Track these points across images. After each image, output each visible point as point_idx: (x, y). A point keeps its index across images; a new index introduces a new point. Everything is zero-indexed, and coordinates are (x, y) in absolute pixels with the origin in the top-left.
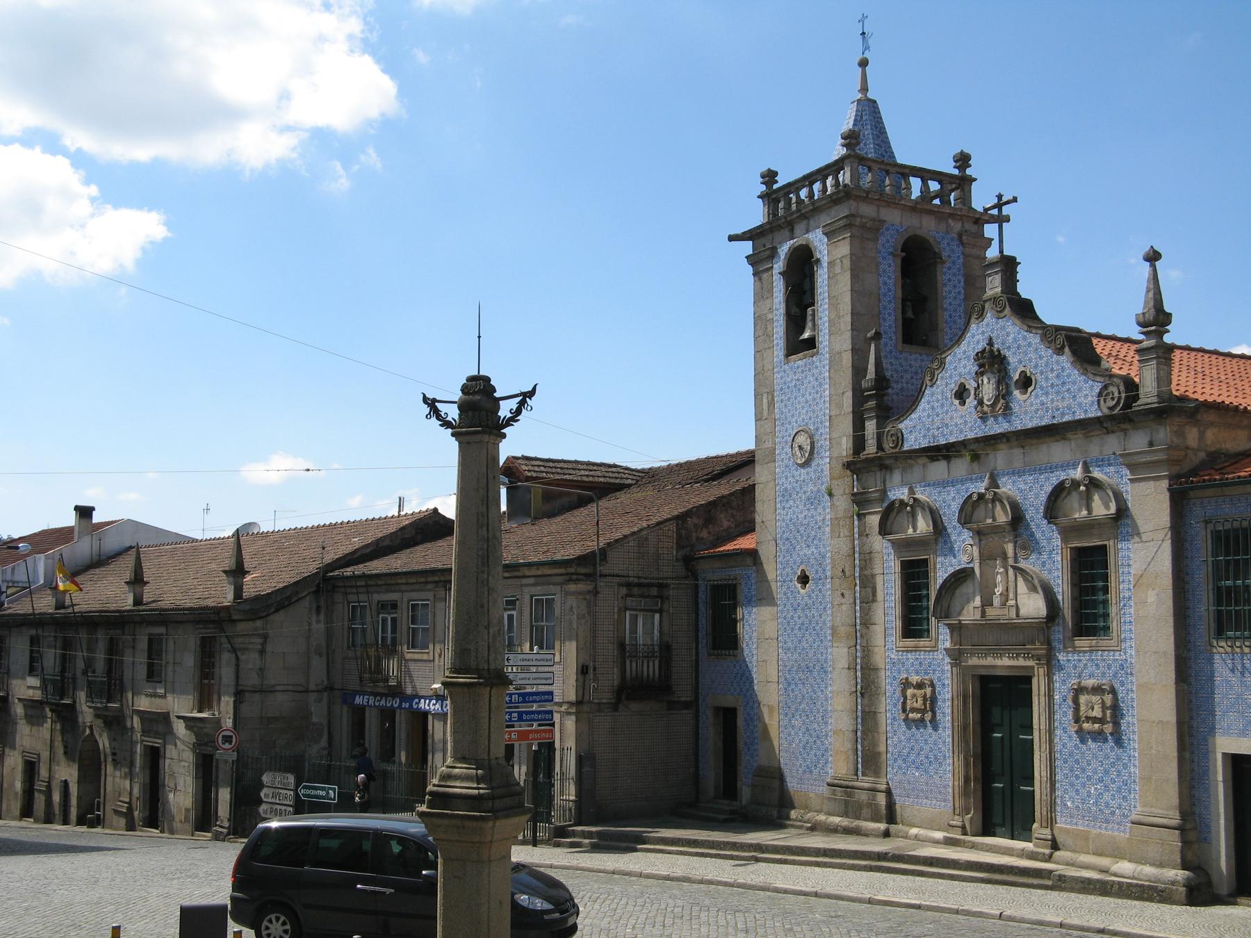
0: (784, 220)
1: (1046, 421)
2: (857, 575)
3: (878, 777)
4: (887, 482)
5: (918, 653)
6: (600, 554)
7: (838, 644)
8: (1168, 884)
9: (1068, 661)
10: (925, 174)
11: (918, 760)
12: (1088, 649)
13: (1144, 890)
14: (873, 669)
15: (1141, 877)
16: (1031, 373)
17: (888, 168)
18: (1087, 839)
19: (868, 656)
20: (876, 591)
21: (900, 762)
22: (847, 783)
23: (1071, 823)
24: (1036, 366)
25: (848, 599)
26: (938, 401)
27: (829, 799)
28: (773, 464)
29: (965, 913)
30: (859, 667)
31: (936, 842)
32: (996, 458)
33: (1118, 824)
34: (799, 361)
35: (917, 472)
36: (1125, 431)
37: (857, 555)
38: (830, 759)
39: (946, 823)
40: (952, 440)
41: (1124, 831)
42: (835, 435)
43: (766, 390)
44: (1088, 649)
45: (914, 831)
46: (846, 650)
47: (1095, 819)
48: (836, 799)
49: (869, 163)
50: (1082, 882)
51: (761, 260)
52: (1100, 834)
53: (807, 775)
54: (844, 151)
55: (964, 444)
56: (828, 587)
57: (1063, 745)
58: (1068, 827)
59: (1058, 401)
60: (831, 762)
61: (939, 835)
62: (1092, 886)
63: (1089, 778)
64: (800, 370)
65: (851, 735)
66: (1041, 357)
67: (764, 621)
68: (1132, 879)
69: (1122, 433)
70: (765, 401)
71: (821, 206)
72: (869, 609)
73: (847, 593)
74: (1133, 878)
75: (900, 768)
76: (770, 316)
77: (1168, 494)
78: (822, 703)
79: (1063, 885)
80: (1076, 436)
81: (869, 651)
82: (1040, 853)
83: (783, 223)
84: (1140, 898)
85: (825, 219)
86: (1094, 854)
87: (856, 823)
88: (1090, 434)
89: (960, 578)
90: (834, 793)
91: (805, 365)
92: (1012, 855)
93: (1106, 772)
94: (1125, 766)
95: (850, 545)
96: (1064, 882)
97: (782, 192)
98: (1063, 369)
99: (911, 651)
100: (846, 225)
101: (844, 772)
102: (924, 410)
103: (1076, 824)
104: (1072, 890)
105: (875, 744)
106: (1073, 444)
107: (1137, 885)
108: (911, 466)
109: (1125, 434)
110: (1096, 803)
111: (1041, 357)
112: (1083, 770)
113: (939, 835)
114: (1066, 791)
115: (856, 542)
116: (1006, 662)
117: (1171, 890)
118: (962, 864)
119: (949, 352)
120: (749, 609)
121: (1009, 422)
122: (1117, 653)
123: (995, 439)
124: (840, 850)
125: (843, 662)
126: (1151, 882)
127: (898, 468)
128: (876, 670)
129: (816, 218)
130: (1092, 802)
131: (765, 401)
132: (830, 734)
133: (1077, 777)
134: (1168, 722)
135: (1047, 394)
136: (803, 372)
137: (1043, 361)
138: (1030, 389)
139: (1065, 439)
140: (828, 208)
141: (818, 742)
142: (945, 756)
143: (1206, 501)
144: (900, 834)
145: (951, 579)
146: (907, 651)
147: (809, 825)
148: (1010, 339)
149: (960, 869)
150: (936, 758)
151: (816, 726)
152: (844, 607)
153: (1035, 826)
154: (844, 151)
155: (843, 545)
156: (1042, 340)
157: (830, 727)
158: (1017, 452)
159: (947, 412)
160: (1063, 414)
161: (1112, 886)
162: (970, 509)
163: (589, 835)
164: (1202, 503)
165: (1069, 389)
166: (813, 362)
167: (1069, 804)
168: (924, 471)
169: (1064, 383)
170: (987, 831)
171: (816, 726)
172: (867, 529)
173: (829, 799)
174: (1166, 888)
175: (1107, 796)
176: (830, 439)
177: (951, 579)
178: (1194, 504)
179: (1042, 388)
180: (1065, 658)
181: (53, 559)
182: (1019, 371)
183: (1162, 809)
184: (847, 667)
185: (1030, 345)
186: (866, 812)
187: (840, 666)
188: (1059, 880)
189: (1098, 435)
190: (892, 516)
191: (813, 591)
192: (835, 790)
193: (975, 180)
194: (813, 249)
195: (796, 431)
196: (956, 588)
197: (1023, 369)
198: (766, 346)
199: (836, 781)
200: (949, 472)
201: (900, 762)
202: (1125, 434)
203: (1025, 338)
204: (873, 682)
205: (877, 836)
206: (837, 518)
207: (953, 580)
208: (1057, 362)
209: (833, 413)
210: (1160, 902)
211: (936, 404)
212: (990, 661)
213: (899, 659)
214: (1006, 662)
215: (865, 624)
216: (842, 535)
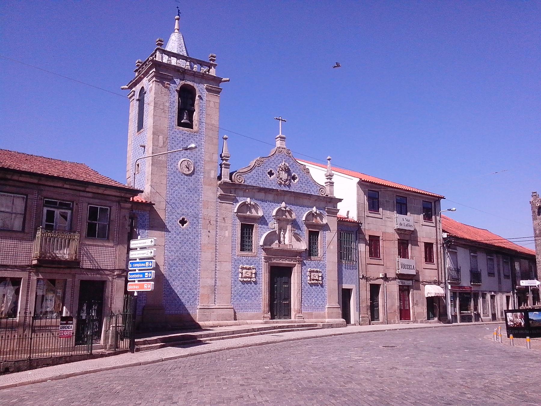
6: (245, 221)
23: (306, 311)
29: (4, 388)
40: (267, 187)
47: (314, 308)
63: (312, 297)
93: (318, 295)
94: (323, 293)
103: (308, 311)
114: (305, 301)
120: (143, 231)
121: (289, 188)
134: (336, 280)
142: (259, 293)
150: (255, 294)
160: (307, 192)
163: (156, 341)
165: (309, 185)
167: (306, 305)
169: (308, 183)
170: (273, 317)
181: (359, 238)
201: (238, 297)
205: (494, 302)
214: (287, 262)
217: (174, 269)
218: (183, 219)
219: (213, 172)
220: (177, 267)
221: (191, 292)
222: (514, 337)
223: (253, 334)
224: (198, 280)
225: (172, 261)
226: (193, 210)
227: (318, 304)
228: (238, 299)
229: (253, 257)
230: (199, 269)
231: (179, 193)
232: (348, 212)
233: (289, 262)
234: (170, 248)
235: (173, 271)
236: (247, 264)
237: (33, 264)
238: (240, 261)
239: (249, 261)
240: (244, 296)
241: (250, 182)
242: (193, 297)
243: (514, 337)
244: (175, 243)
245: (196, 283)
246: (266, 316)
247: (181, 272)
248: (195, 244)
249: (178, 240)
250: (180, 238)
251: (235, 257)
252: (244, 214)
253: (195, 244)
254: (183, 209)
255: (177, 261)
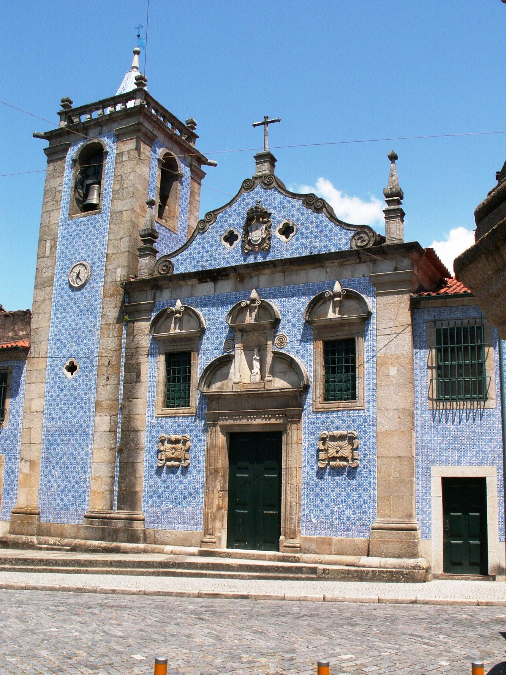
0: (82, 126)
1: (306, 253)
2: (123, 364)
3: (134, 510)
4: (157, 298)
5: (177, 418)
7: (100, 414)
8: (411, 569)
9: (317, 418)
10: (176, 123)
11: (173, 496)
12: (336, 409)
13: (393, 575)
14: (133, 431)
15: (387, 566)
16: (293, 224)
17: (158, 108)
18: (330, 544)
19: (129, 421)
20: (140, 375)
21: (155, 498)
22: (105, 515)
24: (298, 220)
25: (113, 380)
26: (208, 243)
27: (87, 528)
28: (51, 288)
30: (119, 430)
31: (193, 555)
32: (259, 280)
33: (358, 531)
34: (82, 218)
35: (185, 291)
36: (374, 261)
37: (123, 350)
38: (87, 498)
39: (200, 541)
41: (363, 536)
42: (110, 267)
43: (50, 238)
44: (336, 409)
45: (168, 548)
46: (109, 418)
48: (93, 528)
49: (149, 100)
50: (343, 573)
51: (57, 152)
52: (342, 540)
53: (63, 512)
54: (136, 87)
55: (234, 269)
56: (94, 373)
57: (310, 479)
58: (313, 536)
59: (316, 242)
60: (88, 501)
61: (195, 550)
62: (350, 575)
63: (333, 500)
64: (82, 224)
65: (109, 480)
66: (302, 214)
67: (32, 399)
68: (379, 568)
69: (371, 264)
70: (48, 244)
71: (117, 117)
72: (133, 388)
73: (112, 377)
74: (381, 567)
75: (155, 502)
76: (60, 188)
77: (409, 302)
78: (82, 458)
79: (327, 576)
80: (332, 265)
81: (130, 418)
82: (291, 557)
83: (81, 128)
84: (390, 580)
85: (116, 127)
86: (336, 554)
87: (115, 544)
88: (345, 263)
89: (223, 362)
90: (91, 523)
91: (88, 220)
92: (265, 560)
95: (118, 342)
96: (328, 574)
97: (78, 112)
98: (321, 222)
99: (170, 417)
100: (136, 130)
101: (101, 507)
102: (195, 249)
104: (334, 579)
105: (132, 485)
106: (328, 270)
107: (387, 572)
108: (181, 286)
109: (374, 264)
110: (339, 518)
111: (302, 214)
112: (328, 495)
113: (195, 550)
115: (124, 341)
116: (259, 421)
117: (414, 573)
118: (235, 567)
119: (221, 211)
122: (362, 412)
123: (262, 266)
124: (125, 561)
125: (106, 427)
126: (395, 568)
127: (168, 288)
128: (136, 431)
129: (109, 126)
130: (334, 517)
131: (48, 244)
132: (88, 480)
133: (322, 500)
135: (306, 238)
136: (85, 225)
137: (304, 217)
138: (291, 235)
139: (322, 267)
140: (120, 120)
141: (76, 486)
143: (431, 310)
144: (156, 551)
145: (215, 363)
146: (166, 417)
147: (69, 548)
148: (276, 202)
149: (233, 571)
151: (75, 474)
152: (109, 387)
153: (282, 538)
154: (136, 87)
155: (111, 343)
156: (303, 203)
157: (88, 476)
158: (279, 277)
159: (216, 250)
161: (367, 574)
162: (236, 313)
164: (428, 311)
166: (95, 219)
167: (314, 520)
168: (192, 290)
171: (75, 474)
172: (135, 331)
173: (87, 528)
174: (410, 572)
175: (348, 513)
176: (106, 269)
177: (215, 363)
178: (423, 311)
179: (302, 234)
180: (314, 417)
182: (283, 223)
183: (399, 518)
184: (108, 430)
185: (293, 206)
186: (121, 535)
187: (102, 429)
188: (324, 573)
189: (351, 264)
190: (161, 320)
191: (80, 376)
192: (92, 521)
193: (198, 137)
194: (104, 146)
195: (75, 265)
196: (218, 370)
197: (287, 221)
198: (54, 208)
199: (93, 514)
200: (215, 290)
201: (155, 498)
202: (374, 264)
203: (289, 202)
204: (132, 441)
206: (107, 324)
207: (217, 363)
208: (317, 218)
209: (110, 252)
210: (404, 582)
211: (206, 245)
212: (244, 421)
213: (158, 423)
214: (259, 421)
215: (128, 399)
216: (111, 336)
217: (55, 449)
218: (72, 363)
219: (119, 270)
220: (58, 444)
221: (77, 486)
222: (415, 347)
223: (182, 573)
224: (89, 465)
225: (52, 435)
226: (86, 345)
227: (348, 519)
228: (155, 502)
229: (188, 417)
230: (90, 447)
231: (67, 321)
232: (35, 136)
233: (264, 422)
234: (50, 414)
235: (53, 452)
236: (175, 432)
237: (360, 562)
238: (162, 427)
239: (179, 426)
240: (168, 498)
241: (186, 268)
242: (80, 496)
243: (415, 347)
244: (58, 405)
245: (85, 472)
246: (207, 540)
247: (65, 454)
248: (85, 403)
249: (61, 400)
250: (65, 395)
251: (153, 421)
252: (166, 334)
253: (85, 403)
254: (72, 346)
255: (59, 436)
